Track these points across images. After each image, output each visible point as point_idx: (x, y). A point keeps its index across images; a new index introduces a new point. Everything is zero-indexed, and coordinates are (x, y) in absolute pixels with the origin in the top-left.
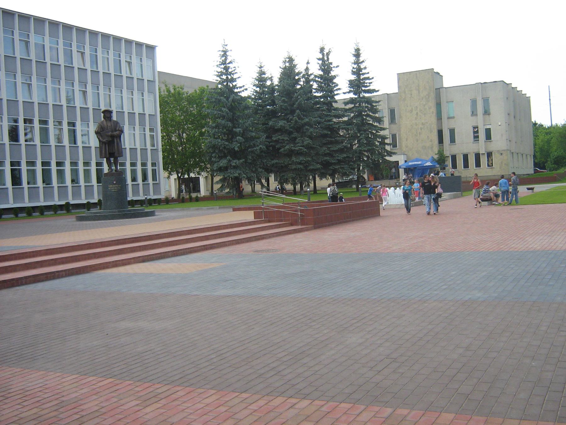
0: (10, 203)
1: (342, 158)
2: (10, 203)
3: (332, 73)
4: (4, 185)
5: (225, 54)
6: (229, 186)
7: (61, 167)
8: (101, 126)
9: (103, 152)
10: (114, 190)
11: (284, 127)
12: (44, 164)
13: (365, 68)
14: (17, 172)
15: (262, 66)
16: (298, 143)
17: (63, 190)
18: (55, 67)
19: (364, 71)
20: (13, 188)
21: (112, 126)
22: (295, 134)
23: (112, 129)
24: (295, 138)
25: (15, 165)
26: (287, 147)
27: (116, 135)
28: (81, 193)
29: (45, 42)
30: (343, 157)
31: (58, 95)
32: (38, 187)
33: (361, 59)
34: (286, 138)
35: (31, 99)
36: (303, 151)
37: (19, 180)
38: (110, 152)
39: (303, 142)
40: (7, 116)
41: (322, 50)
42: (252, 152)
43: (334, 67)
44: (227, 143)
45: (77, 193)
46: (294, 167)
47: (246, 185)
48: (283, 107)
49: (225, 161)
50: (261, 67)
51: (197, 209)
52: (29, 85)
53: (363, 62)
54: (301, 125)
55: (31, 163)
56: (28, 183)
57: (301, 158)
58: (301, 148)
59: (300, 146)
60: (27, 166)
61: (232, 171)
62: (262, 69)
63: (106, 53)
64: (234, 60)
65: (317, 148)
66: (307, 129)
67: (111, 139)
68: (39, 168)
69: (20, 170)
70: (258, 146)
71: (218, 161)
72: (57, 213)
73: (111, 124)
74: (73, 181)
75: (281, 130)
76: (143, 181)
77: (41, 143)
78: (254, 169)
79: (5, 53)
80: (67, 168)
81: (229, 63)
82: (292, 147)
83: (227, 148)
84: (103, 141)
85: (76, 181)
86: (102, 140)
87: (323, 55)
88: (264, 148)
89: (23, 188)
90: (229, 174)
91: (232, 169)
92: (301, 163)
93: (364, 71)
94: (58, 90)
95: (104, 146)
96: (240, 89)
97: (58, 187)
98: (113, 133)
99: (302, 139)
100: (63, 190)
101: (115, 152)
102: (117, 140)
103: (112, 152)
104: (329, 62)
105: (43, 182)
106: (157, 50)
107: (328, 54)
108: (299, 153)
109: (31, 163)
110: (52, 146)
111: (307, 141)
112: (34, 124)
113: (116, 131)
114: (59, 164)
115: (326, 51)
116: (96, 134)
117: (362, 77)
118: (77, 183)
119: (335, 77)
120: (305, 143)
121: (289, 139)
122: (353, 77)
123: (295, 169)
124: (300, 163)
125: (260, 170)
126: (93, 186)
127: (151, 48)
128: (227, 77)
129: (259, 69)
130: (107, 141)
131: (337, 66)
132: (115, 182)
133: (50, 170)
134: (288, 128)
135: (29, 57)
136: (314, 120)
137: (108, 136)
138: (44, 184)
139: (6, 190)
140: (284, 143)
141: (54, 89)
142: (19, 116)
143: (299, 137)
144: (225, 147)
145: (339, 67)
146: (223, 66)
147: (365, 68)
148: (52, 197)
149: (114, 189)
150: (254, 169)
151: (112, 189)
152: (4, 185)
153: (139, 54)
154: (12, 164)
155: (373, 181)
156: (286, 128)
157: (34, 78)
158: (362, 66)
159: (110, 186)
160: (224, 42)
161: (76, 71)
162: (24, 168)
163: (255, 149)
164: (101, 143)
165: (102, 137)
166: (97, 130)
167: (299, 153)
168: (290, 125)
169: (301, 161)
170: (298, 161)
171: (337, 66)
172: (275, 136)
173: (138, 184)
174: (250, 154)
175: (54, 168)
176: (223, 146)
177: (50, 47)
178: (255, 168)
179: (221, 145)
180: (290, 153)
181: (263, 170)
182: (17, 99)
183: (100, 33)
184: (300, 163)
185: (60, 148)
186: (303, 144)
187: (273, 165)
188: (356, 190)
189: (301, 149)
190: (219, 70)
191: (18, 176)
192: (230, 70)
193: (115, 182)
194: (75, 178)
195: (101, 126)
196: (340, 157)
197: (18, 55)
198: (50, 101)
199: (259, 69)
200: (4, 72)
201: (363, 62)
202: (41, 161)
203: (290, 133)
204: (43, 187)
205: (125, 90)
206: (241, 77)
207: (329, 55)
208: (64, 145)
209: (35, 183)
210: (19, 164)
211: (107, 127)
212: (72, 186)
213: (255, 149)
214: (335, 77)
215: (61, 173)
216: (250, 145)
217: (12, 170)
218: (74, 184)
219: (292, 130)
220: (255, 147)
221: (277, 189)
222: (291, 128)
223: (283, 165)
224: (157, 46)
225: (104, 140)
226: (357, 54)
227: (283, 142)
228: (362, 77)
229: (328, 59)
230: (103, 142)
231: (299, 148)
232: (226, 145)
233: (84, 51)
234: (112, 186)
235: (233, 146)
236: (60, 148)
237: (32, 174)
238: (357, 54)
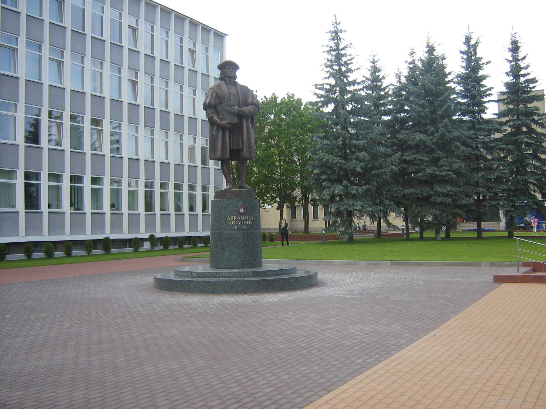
0: (20, 234)
1: (501, 189)
2: (20, 235)
3: (481, 73)
4: (13, 207)
5: (336, 36)
6: (344, 223)
7: (96, 185)
8: (217, 93)
9: (219, 146)
10: (239, 227)
11: (425, 142)
12: (73, 179)
13: (527, 67)
14: (34, 189)
15: (376, 60)
16: (443, 166)
17: (98, 217)
18: (98, 42)
19: (523, 72)
20: (26, 212)
21: (239, 94)
22: (439, 154)
23: (239, 100)
24: (438, 159)
25: (32, 178)
26: (428, 171)
27: (247, 111)
28: (139, 224)
29: (86, 6)
30: (503, 189)
31: (98, 83)
32: (104, 214)
33: (521, 56)
34: (426, 159)
35: (61, 84)
36: (451, 177)
37: (36, 202)
38: (231, 147)
39: (451, 165)
40: (24, 104)
41: (468, 40)
42: (377, 175)
43: (483, 64)
44: (344, 162)
45: (116, 225)
46: (439, 200)
47: (301, 220)
48: (422, 114)
49: (341, 187)
50: (374, 62)
51: (346, 264)
52: (60, 64)
53: (524, 58)
54: (448, 141)
55: (55, 177)
56: (50, 206)
57: (449, 188)
58: (449, 173)
59: (446, 170)
60: (49, 181)
61: (351, 202)
62: (376, 64)
63: (165, 34)
64: (351, 44)
65: (467, 174)
66: (456, 146)
67: (236, 121)
68: (66, 185)
69: (38, 186)
70: (386, 167)
71: (330, 187)
72: (91, 254)
73: (237, 91)
74: (112, 206)
75: (418, 147)
76: (203, 211)
77: (71, 148)
78: (378, 201)
79: (26, 77)
80: (106, 188)
81: (343, 49)
82: (435, 170)
83: (343, 168)
84: (221, 123)
85: (116, 207)
86: (218, 121)
87: (469, 46)
88: (396, 170)
89: (42, 213)
90: (347, 206)
91: (349, 199)
92: (449, 195)
93: (523, 72)
94: (98, 75)
95: (220, 134)
96: (359, 86)
97: (92, 213)
98: (241, 109)
99: (449, 160)
100: (98, 217)
101: (242, 150)
102: (247, 123)
103: (235, 147)
104: (477, 57)
105: (71, 206)
106: (227, 39)
107: (475, 46)
108: (443, 181)
109: (55, 177)
110: (86, 155)
111: (458, 164)
112: (63, 120)
113: (247, 104)
114: (95, 180)
115: (473, 42)
116: (204, 109)
117: (522, 79)
118: (118, 209)
119: (484, 77)
120: (455, 166)
121: (429, 160)
122: (509, 79)
123: (441, 203)
124: (446, 195)
125: (387, 202)
126: (169, 215)
127: (220, 36)
128: (340, 69)
129: (371, 64)
130: (228, 123)
131: (489, 62)
132: (242, 211)
133: (81, 189)
134: (430, 144)
135: (62, 22)
136: (468, 134)
137: (231, 113)
138: (73, 208)
139: (16, 214)
140: (422, 164)
141: (94, 74)
142: (42, 107)
143: (444, 158)
144: (341, 166)
145: (491, 63)
146: (334, 53)
147: (527, 67)
148: (82, 229)
149: (241, 225)
150: (378, 201)
151: (236, 225)
152: (13, 207)
153: (206, 43)
154: (27, 176)
155: (462, 222)
156: (427, 144)
157: (67, 53)
158: (522, 64)
159: (232, 218)
160: (336, 19)
161: (125, 52)
162: (44, 183)
163: (384, 170)
164: (215, 128)
165: (218, 114)
166: (207, 102)
167: (443, 181)
168: (431, 140)
169: (448, 191)
170: (444, 191)
171: (489, 62)
172: (407, 154)
173: (197, 215)
174: (375, 178)
175: (87, 185)
176: (339, 165)
177: (93, 14)
178: (380, 199)
179: (336, 163)
180: (431, 181)
181: (392, 203)
182: (41, 80)
183: (160, 6)
184: (446, 195)
185: (98, 158)
186: (451, 167)
187: (403, 196)
188: (476, 236)
189: (449, 175)
190: (330, 57)
191: (35, 195)
192: (344, 59)
193: (242, 211)
194: (115, 203)
195: (217, 93)
196: (499, 189)
197: (47, 17)
198: (88, 90)
199: (371, 64)
200: (25, 39)
201: (524, 58)
202: (69, 174)
203: (432, 151)
204: (71, 213)
205: (186, 87)
206: (361, 67)
207: (477, 47)
208: (104, 154)
209: (59, 206)
210: (37, 176)
211: (230, 97)
212: (175, 214)
213: (384, 170)
214: (484, 77)
215: (96, 194)
216: (374, 165)
217: (27, 186)
218: (113, 210)
219: (434, 147)
220: (382, 169)
221: (356, 229)
222: (433, 144)
223: (420, 196)
224: (227, 35)
225: (224, 122)
226: (515, 48)
227: (420, 163)
228: (522, 79)
229: (475, 53)
230: (223, 128)
231: (446, 174)
232: (343, 164)
233: (137, 27)
234: (235, 218)
235: (353, 166)
236: (98, 158)
237: (55, 192)
238: (515, 48)
